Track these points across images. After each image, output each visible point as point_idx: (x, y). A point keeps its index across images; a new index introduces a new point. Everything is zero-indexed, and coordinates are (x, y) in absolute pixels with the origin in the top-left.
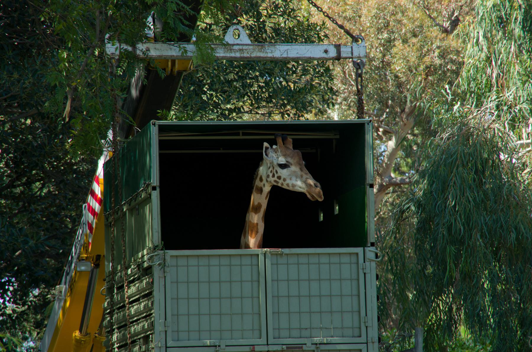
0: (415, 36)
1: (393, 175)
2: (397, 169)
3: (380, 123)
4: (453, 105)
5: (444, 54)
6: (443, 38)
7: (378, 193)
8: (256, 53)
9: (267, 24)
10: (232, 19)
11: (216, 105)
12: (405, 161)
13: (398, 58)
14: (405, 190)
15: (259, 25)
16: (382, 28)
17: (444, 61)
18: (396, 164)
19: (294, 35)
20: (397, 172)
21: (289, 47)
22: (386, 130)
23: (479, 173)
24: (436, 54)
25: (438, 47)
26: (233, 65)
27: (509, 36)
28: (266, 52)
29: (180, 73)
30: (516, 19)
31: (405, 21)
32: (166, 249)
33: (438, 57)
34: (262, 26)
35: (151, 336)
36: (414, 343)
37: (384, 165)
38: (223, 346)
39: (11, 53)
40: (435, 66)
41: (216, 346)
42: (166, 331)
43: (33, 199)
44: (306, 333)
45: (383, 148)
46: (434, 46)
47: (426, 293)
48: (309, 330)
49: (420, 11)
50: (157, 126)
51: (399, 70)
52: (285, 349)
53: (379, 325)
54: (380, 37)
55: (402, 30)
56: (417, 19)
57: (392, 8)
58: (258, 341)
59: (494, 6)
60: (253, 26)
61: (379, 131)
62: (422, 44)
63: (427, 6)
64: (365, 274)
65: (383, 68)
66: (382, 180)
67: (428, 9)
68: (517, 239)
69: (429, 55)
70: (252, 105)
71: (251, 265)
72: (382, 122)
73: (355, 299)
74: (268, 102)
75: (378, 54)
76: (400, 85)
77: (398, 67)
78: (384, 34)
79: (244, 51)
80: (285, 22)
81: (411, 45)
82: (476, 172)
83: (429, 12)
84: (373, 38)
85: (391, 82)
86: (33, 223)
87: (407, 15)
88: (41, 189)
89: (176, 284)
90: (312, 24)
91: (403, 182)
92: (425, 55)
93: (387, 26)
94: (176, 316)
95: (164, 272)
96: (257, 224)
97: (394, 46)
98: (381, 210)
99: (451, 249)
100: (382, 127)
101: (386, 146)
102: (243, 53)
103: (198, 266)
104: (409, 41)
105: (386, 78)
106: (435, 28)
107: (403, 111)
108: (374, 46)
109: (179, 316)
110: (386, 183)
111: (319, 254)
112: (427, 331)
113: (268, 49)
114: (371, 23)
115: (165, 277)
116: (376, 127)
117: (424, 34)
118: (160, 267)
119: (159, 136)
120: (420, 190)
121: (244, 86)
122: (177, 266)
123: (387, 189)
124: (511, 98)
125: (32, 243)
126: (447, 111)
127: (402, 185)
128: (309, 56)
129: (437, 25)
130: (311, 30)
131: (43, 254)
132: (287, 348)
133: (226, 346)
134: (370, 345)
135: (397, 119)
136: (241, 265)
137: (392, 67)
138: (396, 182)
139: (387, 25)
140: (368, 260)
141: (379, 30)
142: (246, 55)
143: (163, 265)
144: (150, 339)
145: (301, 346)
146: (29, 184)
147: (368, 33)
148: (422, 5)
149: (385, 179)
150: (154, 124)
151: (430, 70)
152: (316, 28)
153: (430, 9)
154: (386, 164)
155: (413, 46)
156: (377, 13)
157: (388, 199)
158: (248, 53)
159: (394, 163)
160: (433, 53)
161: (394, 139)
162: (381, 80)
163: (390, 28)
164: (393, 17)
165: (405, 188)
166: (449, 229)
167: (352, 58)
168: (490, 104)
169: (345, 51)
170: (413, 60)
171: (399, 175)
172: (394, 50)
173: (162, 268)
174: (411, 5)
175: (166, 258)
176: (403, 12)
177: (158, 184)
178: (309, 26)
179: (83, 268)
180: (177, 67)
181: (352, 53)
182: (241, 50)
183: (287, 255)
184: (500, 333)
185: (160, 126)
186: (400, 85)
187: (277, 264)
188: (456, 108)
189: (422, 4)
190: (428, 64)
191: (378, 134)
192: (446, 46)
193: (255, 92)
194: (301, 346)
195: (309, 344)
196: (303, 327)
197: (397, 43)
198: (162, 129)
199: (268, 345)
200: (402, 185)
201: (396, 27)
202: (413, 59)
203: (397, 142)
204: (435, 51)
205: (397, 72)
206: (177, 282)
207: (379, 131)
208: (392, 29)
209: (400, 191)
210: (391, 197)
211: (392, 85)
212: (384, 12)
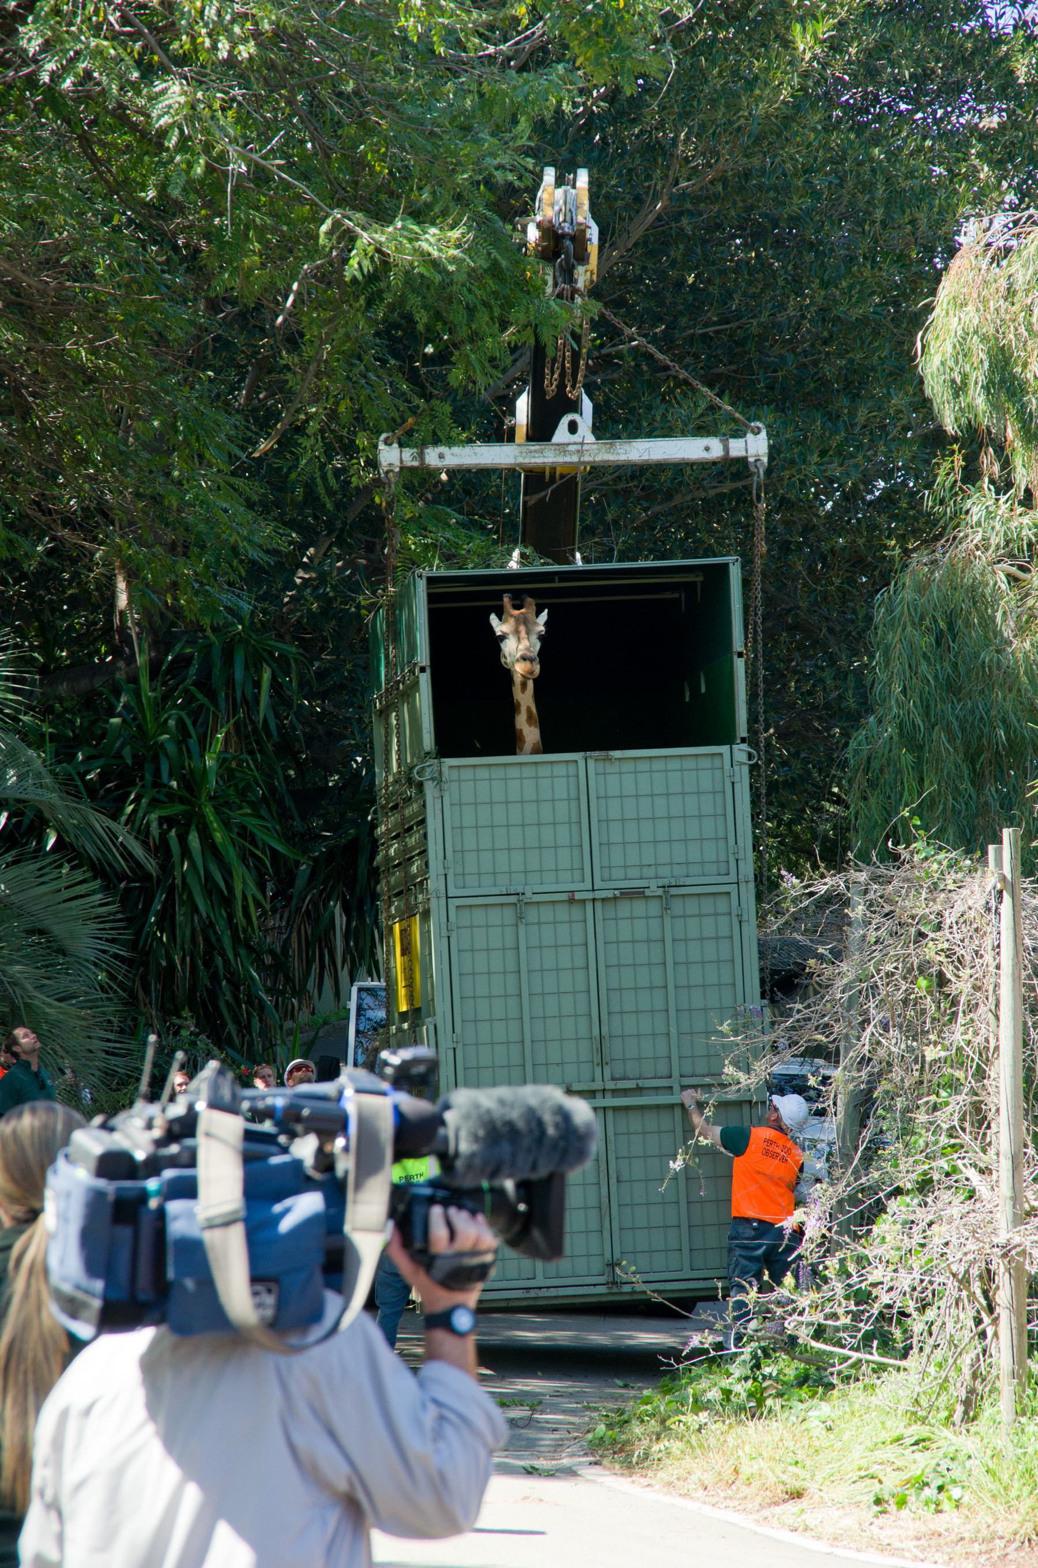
21: (651, 444)
30: (976, 383)
38: (528, 894)
44: (650, 872)
50: (424, 579)
58: (581, 887)
71: (568, 776)
134: (742, 886)
150: (420, 577)
195: (653, 887)
198: (431, 581)
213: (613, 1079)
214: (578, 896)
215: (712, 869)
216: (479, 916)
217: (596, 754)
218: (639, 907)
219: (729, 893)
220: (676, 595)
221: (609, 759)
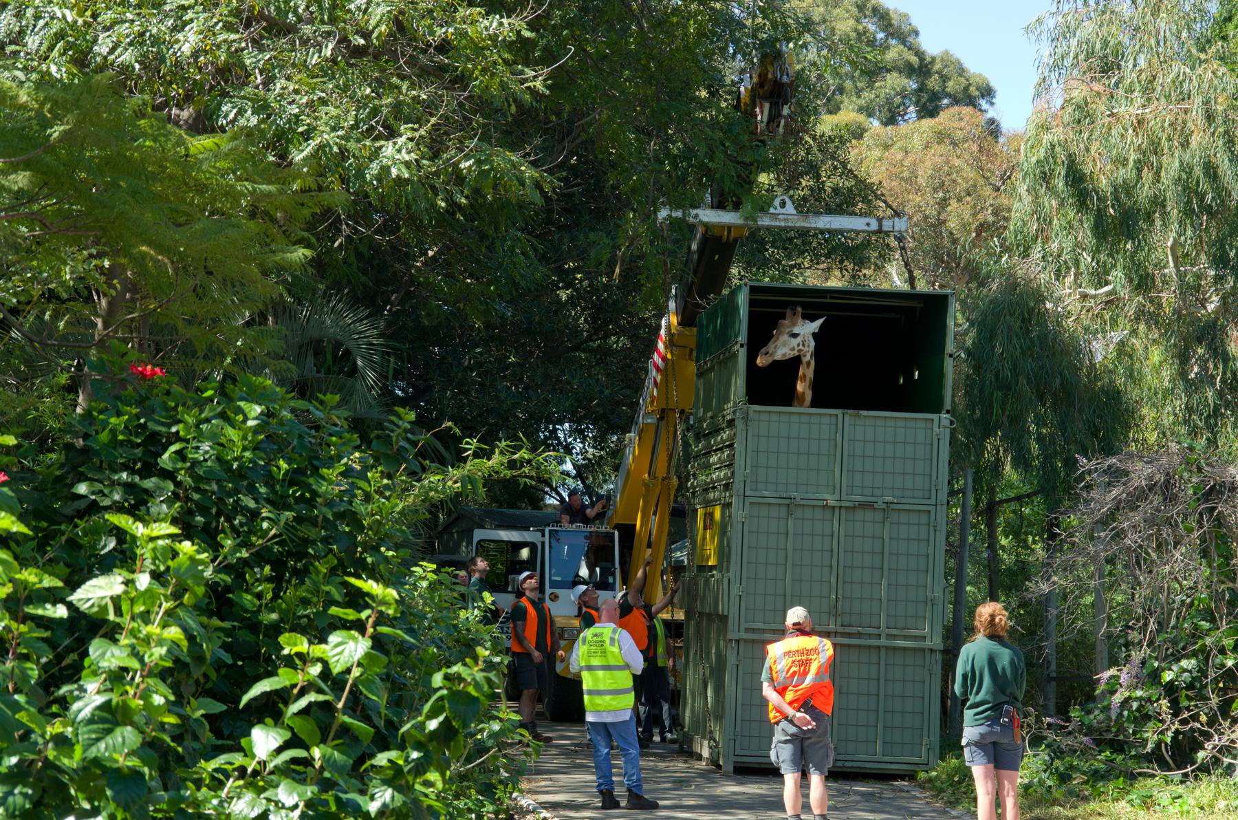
0: (969, 194)
4: (1002, 257)
8: (801, 223)
11: (779, 262)
23: (1026, 321)
24: (989, 211)
25: (991, 205)
27: (1051, 189)
29: (736, 240)
31: (960, 181)
38: (798, 499)
39: (587, 217)
40: (988, 223)
43: (610, 352)
44: (877, 492)
46: (988, 204)
59: (1038, 162)
68: (1062, 384)
70: (811, 261)
74: (827, 258)
77: (953, 224)
82: (1023, 320)
85: (946, 239)
86: (609, 374)
88: (616, 342)
96: (804, 393)
99: (998, 394)
107: (958, 266)
120: (970, 338)
121: (804, 243)
124: (1056, 250)
125: (607, 392)
126: (996, 262)
129: (990, 184)
131: (619, 403)
139: (942, 185)
141: (935, 190)
142: (790, 224)
143: (746, 419)
146: (606, 337)
151: (982, 227)
166: (997, 375)
168: (1036, 253)
172: (949, 209)
176: (957, 172)
179: (649, 421)
180: (733, 235)
182: (786, 220)
184: (1044, 474)
186: (955, 241)
188: (1004, 259)
190: (982, 221)
193: (815, 248)
197: (952, 202)
202: (967, 216)
213: (842, 626)
217: (851, 412)
218: (869, 515)
219: (929, 512)
220: (898, 316)
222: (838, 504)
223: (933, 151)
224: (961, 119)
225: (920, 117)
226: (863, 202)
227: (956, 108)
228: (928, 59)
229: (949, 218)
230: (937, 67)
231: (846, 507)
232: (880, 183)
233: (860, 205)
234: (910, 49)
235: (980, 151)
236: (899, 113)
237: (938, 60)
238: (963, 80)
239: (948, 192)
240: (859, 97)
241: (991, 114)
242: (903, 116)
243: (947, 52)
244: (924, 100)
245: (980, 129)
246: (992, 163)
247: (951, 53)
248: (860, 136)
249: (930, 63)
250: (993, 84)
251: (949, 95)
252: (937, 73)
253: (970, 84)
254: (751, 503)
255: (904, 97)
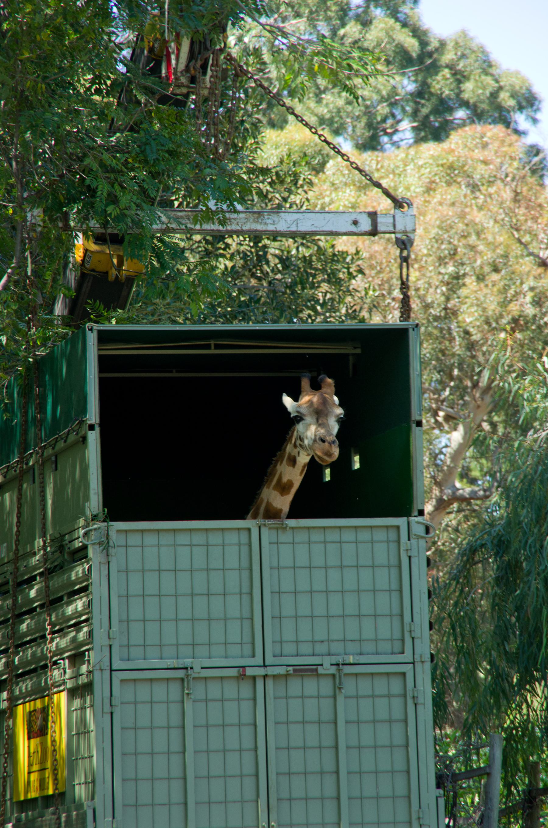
0: (496, 270)
1: (458, 485)
2: (465, 475)
3: (440, 403)
5: (540, 299)
6: (540, 275)
7: (436, 512)
9: (271, 251)
10: (217, 241)
12: (478, 462)
13: (469, 304)
14: (477, 508)
15: (257, 252)
16: (445, 257)
17: (541, 310)
18: (463, 467)
19: (311, 268)
20: (465, 480)
22: (450, 414)
24: (528, 299)
25: (532, 289)
26: (215, 312)
28: (266, 224)
31: (481, 248)
32: (111, 521)
33: (531, 303)
34: (261, 253)
35: (87, 653)
36: (488, 754)
37: (445, 468)
38: (197, 669)
40: (525, 317)
41: (186, 668)
42: (110, 646)
44: (321, 648)
45: (444, 441)
46: (525, 287)
47: (507, 679)
48: (326, 643)
49: (504, 232)
51: (471, 323)
52: (292, 672)
53: (429, 602)
54: (443, 271)
55: (475, 261)
56: (500, 245)
57: (461, 226)
60: (249, 254)
61: (439, 416)
62: (507, 283)
63: (516, 225)
64: (410, 557)
65: (445, 318)
66: (441, 491)
67: (517, 230)
69: (517, 300)
71: (239, 545)
72: (443, 401)
73: (395, 596)
75: (438, 296)
76: (471, 346)
78: (448, 266)
79: (233, 220)
80: (297, 248)
81: (490, 285)
83: (518, 233)
84: (430, 272)
87: (484, 239)
89: (125, 573)
90: (339, 252)
91: (474, 496)
92: (511, 300)
93: (454, 254)
94: (126, 623)
95: (108, 555)
97: (464, 285)
98: (439, 538)
100: (442, 410)
101: (449, 439)
102: (231, 224)
103: (159, 546)
104: (487, 277)
105: (450, 334)
106: (527, 259)
107: (475, 385)
108: (432, 284)
109: (130, 623)
110: (447, 497)
111: (340, 528)
112: (505, 739)
113: (268, 219)
114: (428, 249)
115: (109, 562)
116: (434, 409)
117: (510, 268)
118: (101, 548)
119: (99, 350)
122: (126, 546)
123: (449, 506)
127: (472, 501)
128: (330, 230)
129: (531, 254)
130: (338, 261)
132: (294, 670)
133: (202, 668)
134: (418, 666)
135: (467, 398)
136: (223, 545)
137: (460, 318)
138: (462, 495)
139: (454, 254)
140: (414, 537)
141: (441, 261)
144: (86, 658)
145: (314, 667)
147: (424, 265)
148: (508, 224)
149: (446, 491)
150: (91, 330)
152: (345, 259)
153: (521, 229)
154: (448, 466)
155: (493, 285)
156: (438, 234)
157: (451, 521)
158: (238, 224)
159: (460, 466)
160: (524, 298)
161: (461, 428)
162: (443, 337)
163: (457, 257)
164: (464, 241)
165: (477, 505)
167: (394, 233)
169: (384, 223)
170: (493, 307)
171: (468, 485)
172: (463, 292)
173: (104, 549)
174: (492, 222)
175: (110, 533)
176: (478, 234)
177: (98, 421)
178: (334, 255)
181: (394, 226)
183: (292, 528)
185: (100, 332)
186: (471, 346)
187: (277, 543)
189: (508, 221)
190: (516, 314)
191: (436, 421)
192: (543, 287)
194: (314, 667)
196: (316, 638)
197: (467, 280)
199: (265, 666)
200: (472, 501)
201: (467, 256)
202: (492, 307)
203: (466, 433)
204: (526, 294)
205: (468, 325)
206: (127, 571)
207: (439, 416)
208: (461, 259)
209: (468, 510)
210: (455, 519)
211: (460, 345)
212: (448, 232)
214: (249, 672)
215: (386, 646)
216: (143, 692)
219: (404, 674)
221: (285, 529)
222: (261, 672)
223: (438, 198)
224: (485, 146)
225: (419, 140)
226: (329, 282)
227: (479, 128)
228: (434, 44)
229: (464, 307)
230: (448, 57)
231: (274, 677)
232: (357, 252)
233: (325, 287)
234: (405, 25)
235: (516, 200)
236: (384, 130)
237: (450, 45)
238: (489, 80)
239: (463, 264)
240: (319, 101)
241: (531, 139)
242: (391, 135)
243: (464, 34)
244: (425, 111)
245: (516, 164)
246: (535, 219)
247: (471, 34)
248: (319, 169)
249: (437, 50)
250: (538, 89)
251: (465, 104)
252: (447, 66)
253: (501, 88)
254: (122, 681)
255: (392, 105)
